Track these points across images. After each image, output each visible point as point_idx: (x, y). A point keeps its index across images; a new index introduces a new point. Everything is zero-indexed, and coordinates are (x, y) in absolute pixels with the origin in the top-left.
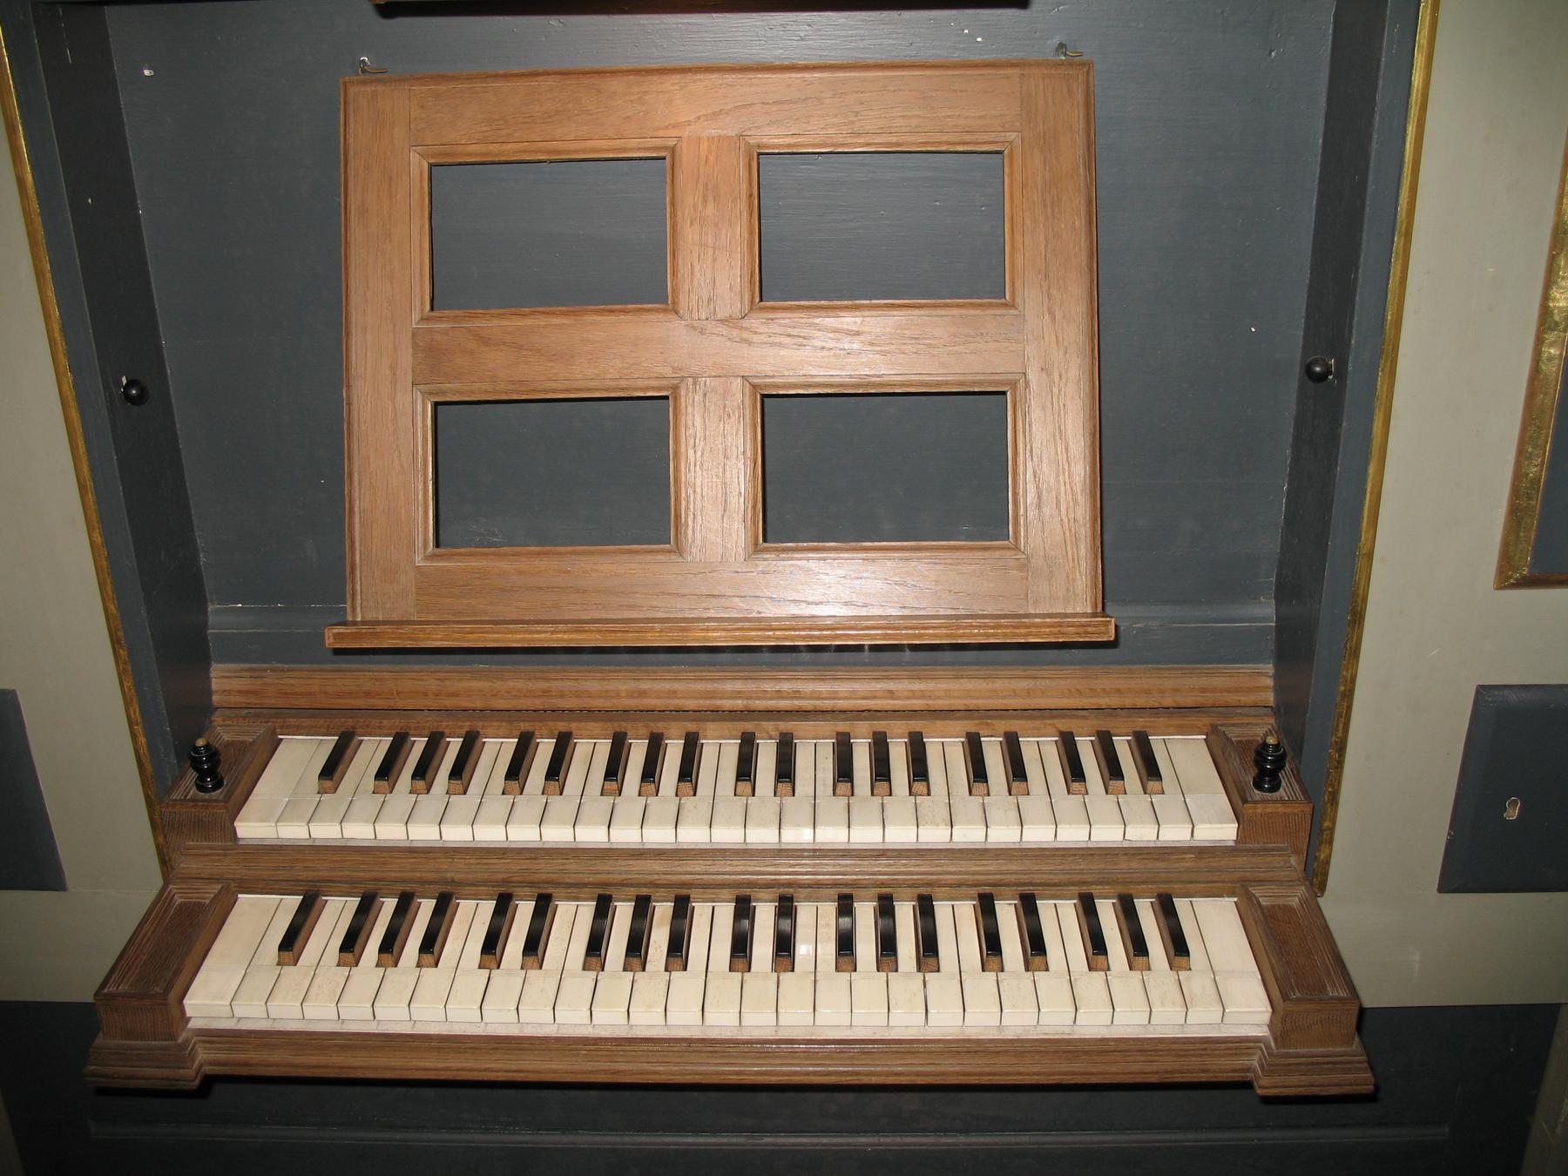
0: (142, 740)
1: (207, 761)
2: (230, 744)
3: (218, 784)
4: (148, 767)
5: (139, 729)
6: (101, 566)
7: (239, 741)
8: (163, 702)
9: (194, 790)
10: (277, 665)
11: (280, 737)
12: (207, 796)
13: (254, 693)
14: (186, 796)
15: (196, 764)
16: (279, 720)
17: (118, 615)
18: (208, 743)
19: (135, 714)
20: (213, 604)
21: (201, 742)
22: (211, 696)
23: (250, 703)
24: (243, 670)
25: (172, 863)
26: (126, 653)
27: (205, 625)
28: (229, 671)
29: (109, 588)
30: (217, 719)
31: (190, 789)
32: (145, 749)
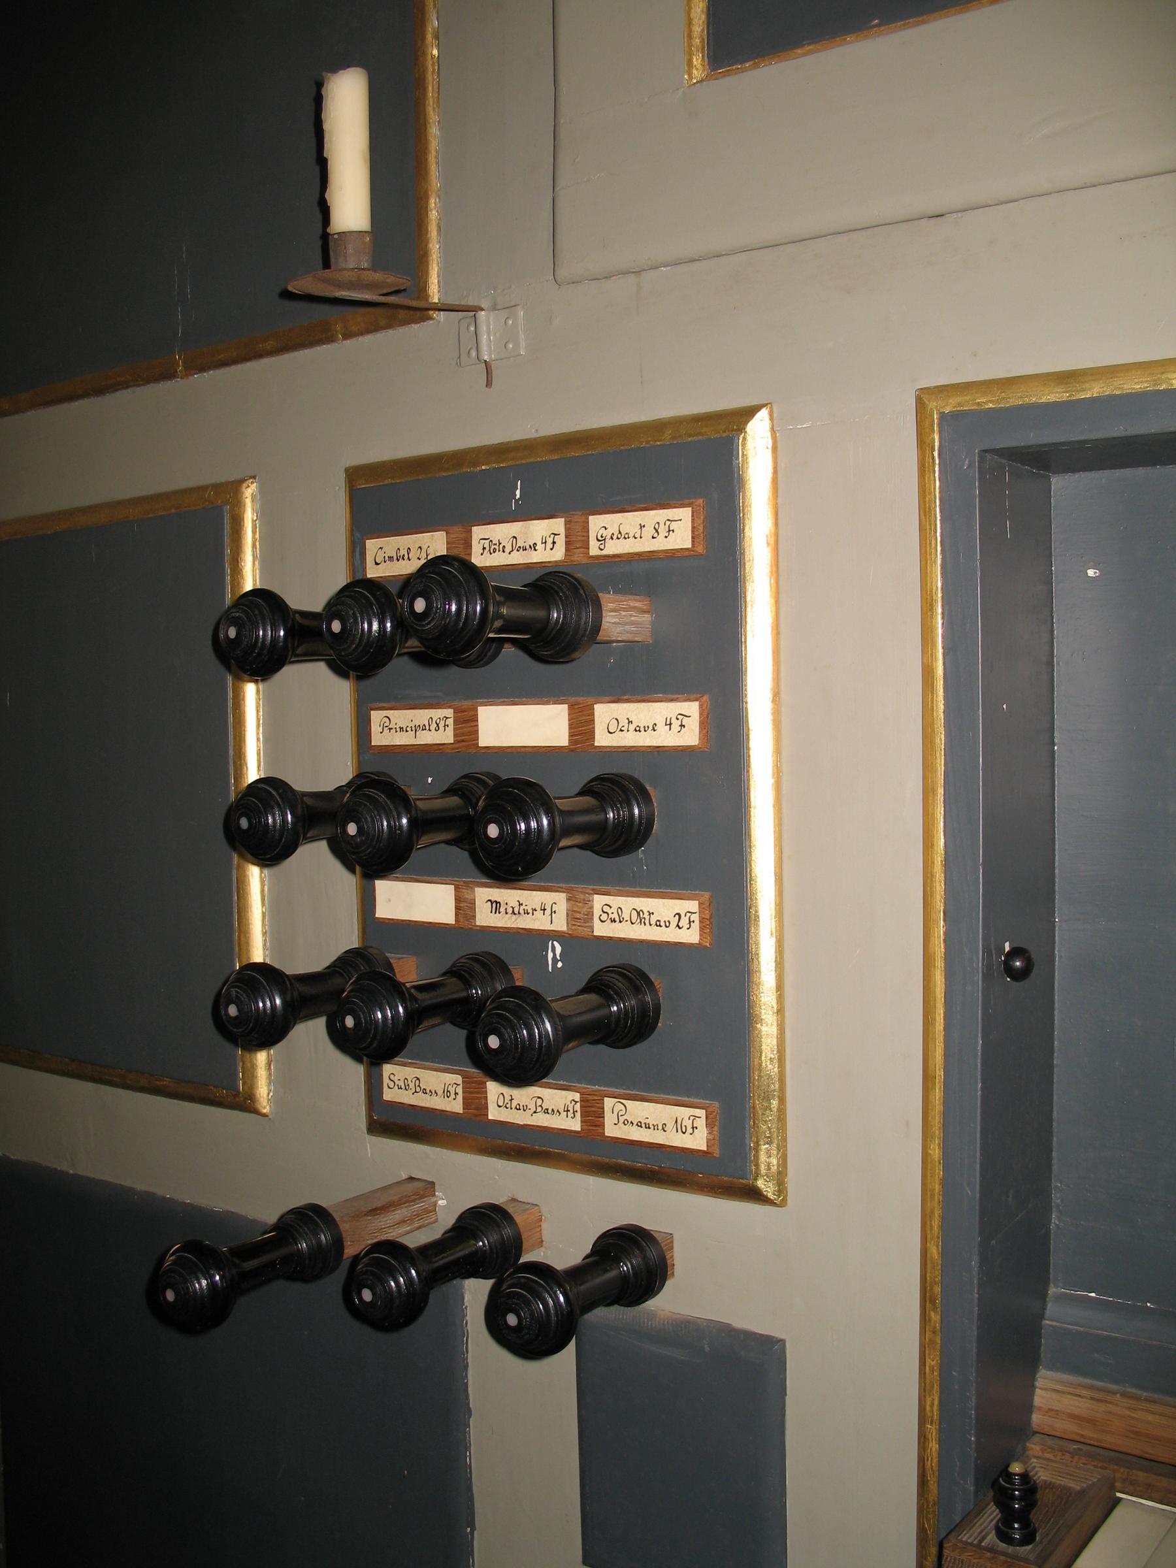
0: (934, 1446)
1: (1020, 1499)
2: (1049, 1485)
3: (1028, 1538)
4: (933, 1486)
5: (932, 1430)
6: (933, 1190)
7: (1060, 1485)
8: (973, 1398)
9: (991, 1538)
10: (1129, 1390)
11: (1118, 1495)
12: (1010, 1549)
13: (1092, 1422)
14: (981, 1541)
15: (1003, 1498)
16: (1122, 1470)
17: (940, 1262)
18: (1026, 1471)
19: (932, 1405)
20: (1056, 1286)
21: (1016, 1468)
22: (1031, 1412)
23: (1082, 1436)
24: (1080, 1386)
25: (439, 255)
26: (939, 1317)
27: (1042, 1316)
28: (1061, 1382)
29: (936, 1223)
30: (1034, 1447)
31: (987, 1534)
32: (935, 1461)
